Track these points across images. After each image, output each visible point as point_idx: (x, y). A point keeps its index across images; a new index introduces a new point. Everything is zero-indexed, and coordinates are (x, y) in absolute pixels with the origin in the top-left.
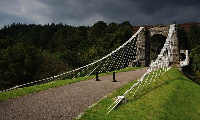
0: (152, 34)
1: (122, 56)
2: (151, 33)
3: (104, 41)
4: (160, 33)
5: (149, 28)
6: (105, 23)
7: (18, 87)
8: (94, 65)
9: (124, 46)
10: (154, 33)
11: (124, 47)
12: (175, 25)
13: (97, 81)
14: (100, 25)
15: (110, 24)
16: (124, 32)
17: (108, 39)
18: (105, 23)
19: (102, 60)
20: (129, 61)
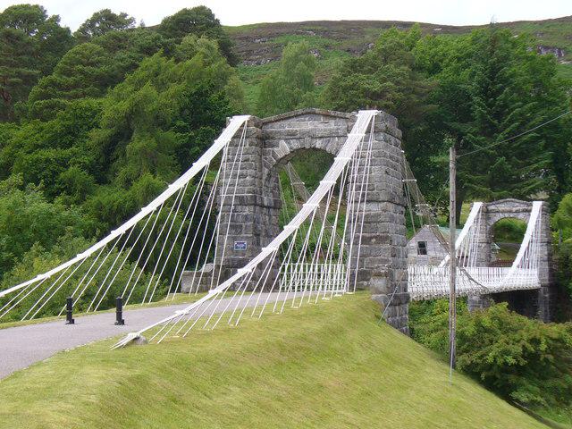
0: (283, 148)
1: (171, 239)
2: (283, 143)
3: (52, 143)
4: (318, 144)
5: (272, 118)
6: (56, 18)
7: (502, 162)
8: (49, 282)
9: (159, 208)
10: (296, 145)
11: (156, 212)
12: (374, 112)
13: (70, 323)
14: (18, 30)
15: (90, 24)
16: (174, 88)
17: (69, 136)
18: (56, 18)
19: (75, 265)
20: (181, 267)
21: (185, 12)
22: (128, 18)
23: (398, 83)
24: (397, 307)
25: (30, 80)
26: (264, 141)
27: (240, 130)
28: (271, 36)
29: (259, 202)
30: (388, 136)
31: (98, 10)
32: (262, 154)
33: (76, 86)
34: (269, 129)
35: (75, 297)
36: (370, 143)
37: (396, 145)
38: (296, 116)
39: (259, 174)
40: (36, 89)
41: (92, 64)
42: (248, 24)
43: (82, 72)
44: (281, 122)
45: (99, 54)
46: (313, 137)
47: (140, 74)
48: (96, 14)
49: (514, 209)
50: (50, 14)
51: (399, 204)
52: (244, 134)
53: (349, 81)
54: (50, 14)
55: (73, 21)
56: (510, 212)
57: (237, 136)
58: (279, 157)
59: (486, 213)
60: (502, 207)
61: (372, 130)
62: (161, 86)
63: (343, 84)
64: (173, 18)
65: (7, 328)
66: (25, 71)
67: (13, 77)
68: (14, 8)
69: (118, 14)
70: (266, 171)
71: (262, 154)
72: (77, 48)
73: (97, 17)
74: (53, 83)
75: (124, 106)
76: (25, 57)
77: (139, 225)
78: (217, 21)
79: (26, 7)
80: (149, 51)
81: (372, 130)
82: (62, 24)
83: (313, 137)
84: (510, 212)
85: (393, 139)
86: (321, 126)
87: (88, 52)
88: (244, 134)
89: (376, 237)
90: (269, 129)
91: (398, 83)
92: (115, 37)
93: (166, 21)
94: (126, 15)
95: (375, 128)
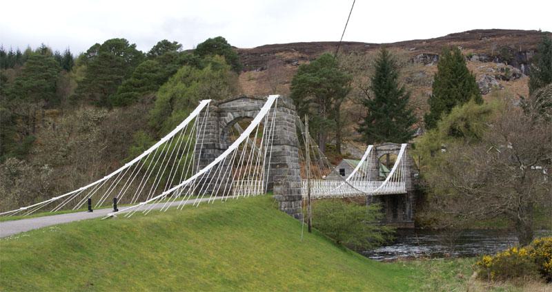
2: (230, 114)
6: (134, 46)
10: (237, 115)
14: (512, 69)
15: (156, 48)
18: (134, 46)
21: (210, 40)
22: (178, 44)
23: (329, 78)
24: (293, 203)
25: (118, 81)
26: (220, 113)
27: (205, 108)
28: (274, 52)
29: (217, 147)
30: (285, 109)
31: (160, 40)
32: (219, 120)
33: (143, 84)
34: (222, 107)
35: (119, 198)
36: (275, 113)
37: (292, 113)
38: (237, 99)
39: (217, 132)
40: (120, 87)
41: (153, 72)
42: (204, 41)
43: (146, 76)
44: (229, 103)
45: (156, 65)
46: (246, 111)
47: (176, 76)
48: (159, 43)
49: (391, 149)
50: (130, 43)
51: (293, 146)
52: (207, 110)
53: (302, 77)
54: (130, 43)
55: (145, 48)
56: (389, 150)
57: (203, 111)
58: (228, 122)
59: (375, 151)
60: (384, 147)
61: (276, 106)
62: (188, 84)
63: (298, 79)
64: (203, 44)
65: (63, 213)
66: (115, 76)
67: (109, 80)
68: (110, 41)
69: (172, 42)
70: (221, 130)
71: (219, 120)
72: (144, 63)
73: (160, 45)
74: (130, 84)
75: (168, 95)
76: (116, 69)
77: (142, 161)
78: (229, 44)
79: (117, 40)
80: (183, 63)
81: (276, 106)
82: (138, 49)
83: (246, 111)
84: (389, 150)
85: (289, 111)
86: (250, 104)
87: (150, 65)
88: (207, 110)
89: (279, 164)
90: (222, 107)
91: (329, 78)
92: (170, 55)
93: (199, 46)
94: (177, 43)
95: (278, 104)
